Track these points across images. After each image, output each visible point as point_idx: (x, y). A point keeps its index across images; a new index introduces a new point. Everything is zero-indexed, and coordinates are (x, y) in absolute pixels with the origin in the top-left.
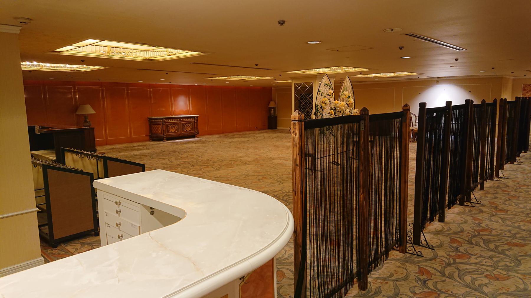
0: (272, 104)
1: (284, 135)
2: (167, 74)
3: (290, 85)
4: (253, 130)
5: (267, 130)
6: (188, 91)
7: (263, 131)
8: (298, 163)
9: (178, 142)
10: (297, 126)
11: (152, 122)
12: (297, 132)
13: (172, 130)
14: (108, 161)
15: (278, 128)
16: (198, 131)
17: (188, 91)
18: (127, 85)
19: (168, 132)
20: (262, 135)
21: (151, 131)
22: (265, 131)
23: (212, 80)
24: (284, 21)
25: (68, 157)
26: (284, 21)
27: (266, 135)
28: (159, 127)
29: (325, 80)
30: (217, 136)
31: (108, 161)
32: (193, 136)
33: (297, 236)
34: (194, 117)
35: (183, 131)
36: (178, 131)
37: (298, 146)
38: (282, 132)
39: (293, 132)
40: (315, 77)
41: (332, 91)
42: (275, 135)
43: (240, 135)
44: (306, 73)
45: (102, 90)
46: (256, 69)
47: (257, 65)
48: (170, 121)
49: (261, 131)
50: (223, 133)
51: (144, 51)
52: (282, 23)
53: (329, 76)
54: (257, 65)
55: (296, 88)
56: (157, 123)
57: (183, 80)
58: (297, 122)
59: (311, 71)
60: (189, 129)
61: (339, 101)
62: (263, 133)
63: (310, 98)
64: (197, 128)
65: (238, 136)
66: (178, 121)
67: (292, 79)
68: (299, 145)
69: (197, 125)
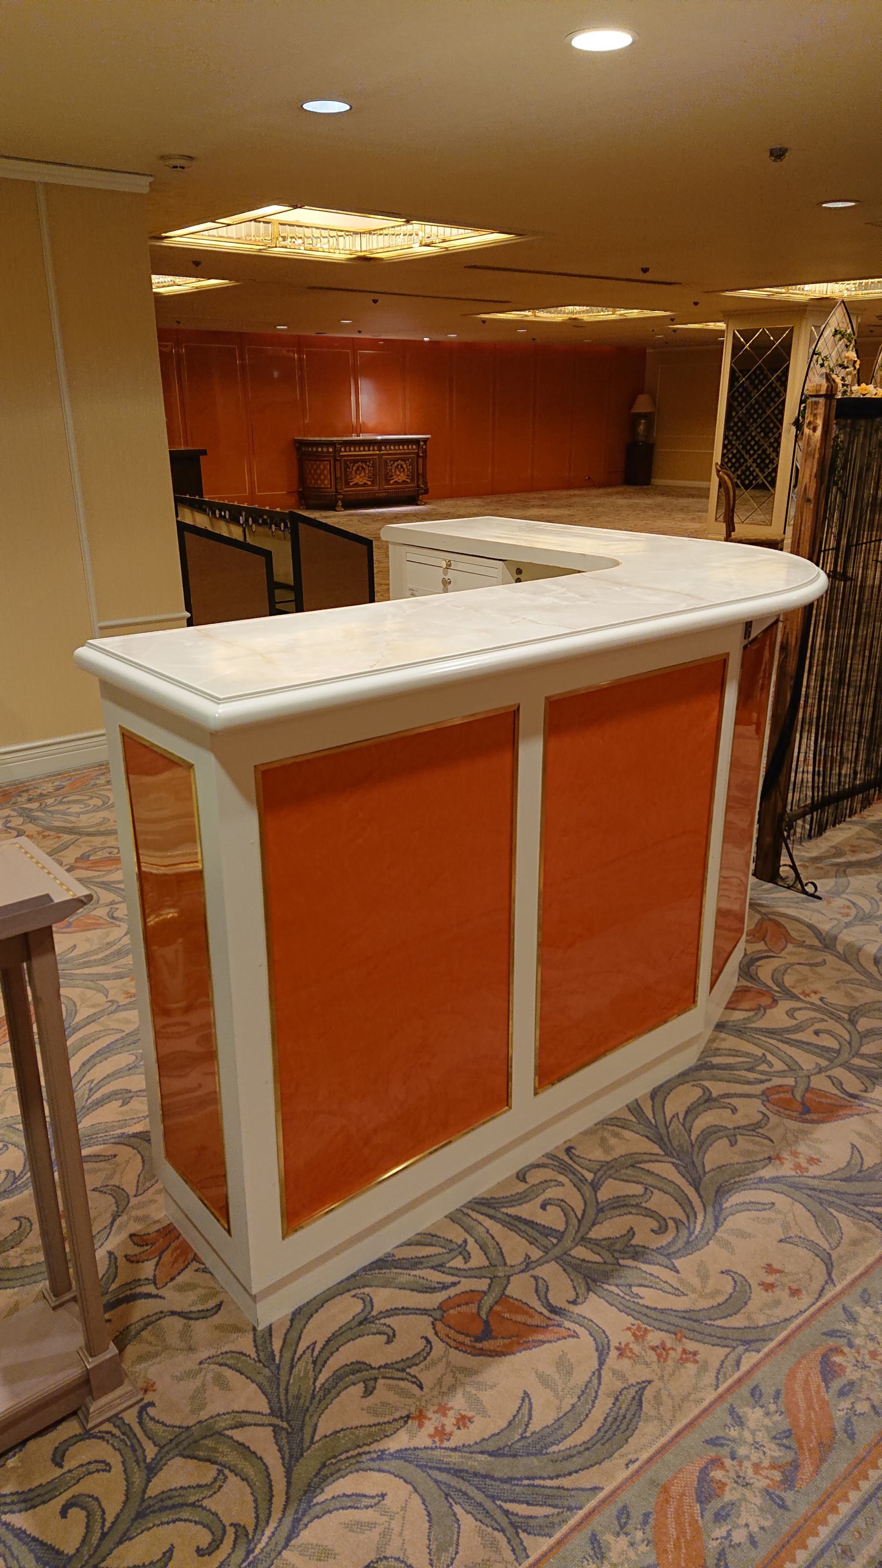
0: (643, 405)
1: (675, 501)
2: (375, 301)
3: (714, 341)
4: (580, 487)
5: (621, 489)
6: (396, 363)
7: (610, 490)
8: (811, 495)
9: (374, 515)
10: (821, 411)
11: (305, 454)
12: (820, 422)
13: (359, 479)
14: (300, 524)
15: (655, 481)
16: (425, 483)
17: (396, 363)
18: (242, 338)
19: (347, 484)
20: (606, 500)
21: (302, 479)
22: (615, 490)
23: (484, 321)
24: (786, 150)
25: (799, 339)
26: (786, 150)
27: (621, 501)
28: (325, 467)
29: (837, 319)
30: (477, 501)
31: (300, 524)
32: (412, 500)
33: (786, 657)
34: (417, 442)
35: (387, 482)
36: (373, 483)
37: (817, 456)
38: (667, 492)
39: (810, 423)
40: (800, 310)
41: (852, 355)
42: (649, 501)
43: (543, 499)
44: (777, 297)
45: (178, 353)
46: (638, 283)
47: (645, 270)
48: (353, 452)
49: (601, 491)
50: (493, 493)
51: (356, 233)
52: (778, 154)
53: (850, 307)
54: (645, 270)
55: (737, 347)
56: (318, 457)
57: (391, 326)
58: (822, 400)
59: (793, 289)
60: (402, 477)
61: (871, 387)
62: (610, 495)
63: (779, 379)
64: (424, 475)
65: (538, 502)
66: (373, 451)
67: (727, 316)
68: (820, 454)
69: (424, 465)
